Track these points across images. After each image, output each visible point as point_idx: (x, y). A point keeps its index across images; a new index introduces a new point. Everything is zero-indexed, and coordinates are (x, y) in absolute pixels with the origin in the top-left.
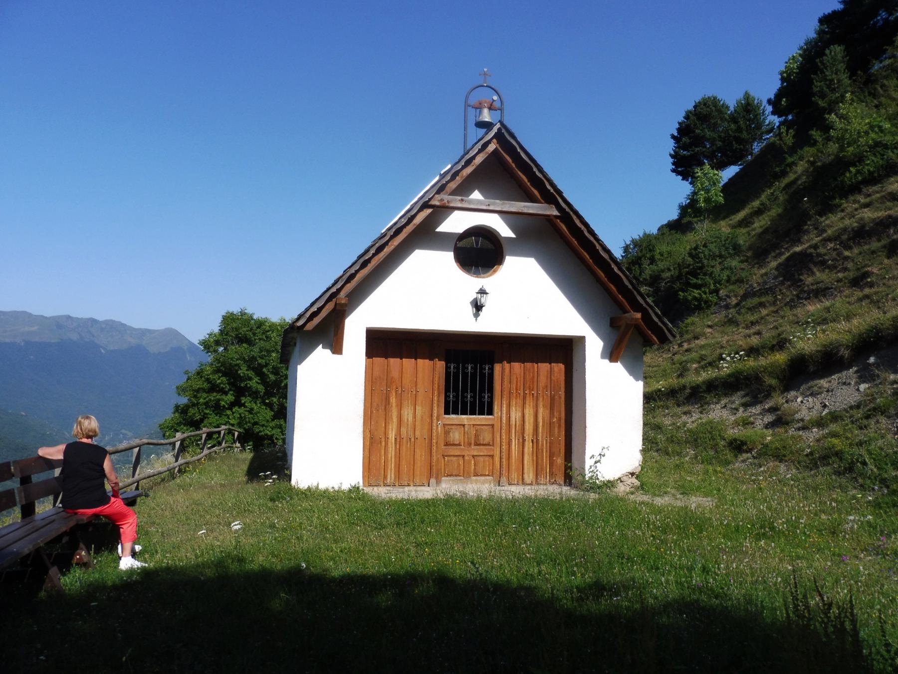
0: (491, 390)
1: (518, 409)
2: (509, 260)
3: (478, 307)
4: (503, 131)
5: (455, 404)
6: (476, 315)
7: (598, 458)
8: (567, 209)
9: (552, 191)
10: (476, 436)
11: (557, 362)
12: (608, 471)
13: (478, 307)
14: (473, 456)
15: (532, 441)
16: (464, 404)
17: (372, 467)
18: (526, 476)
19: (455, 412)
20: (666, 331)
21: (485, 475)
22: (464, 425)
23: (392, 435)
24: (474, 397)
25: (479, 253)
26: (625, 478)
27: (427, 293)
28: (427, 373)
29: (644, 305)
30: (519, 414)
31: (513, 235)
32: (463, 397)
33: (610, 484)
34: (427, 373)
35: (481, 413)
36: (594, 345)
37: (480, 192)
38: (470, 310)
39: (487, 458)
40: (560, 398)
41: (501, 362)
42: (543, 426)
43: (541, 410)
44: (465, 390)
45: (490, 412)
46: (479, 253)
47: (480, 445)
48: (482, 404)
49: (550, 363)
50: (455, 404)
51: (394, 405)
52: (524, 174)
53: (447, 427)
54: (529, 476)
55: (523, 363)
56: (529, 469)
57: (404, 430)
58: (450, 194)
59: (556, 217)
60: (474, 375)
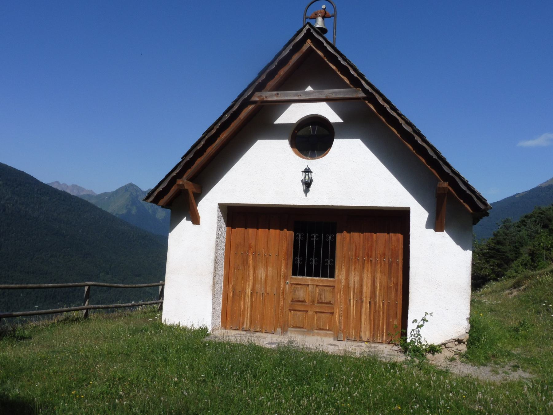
0: (333, 257)
1: (354, 275)
2: (337, 143)
3: (307, 185)
4: (312, 30)
5: (302, 266)
6: (306, 191)
7: (421, 323)
8: (370, 90)
9: (356, 75)
10: (320, 295)
11: (395, 232)
12: (430, 336)
13: (307, 185)
14: (316, 312)
15: (370, 303)
16: (309, 267)
17: (229, 315)
18: (363, 334)
19: (302, 274)
20: (475, 199)
21: (326, 330)
22: (308, 285)
23: (249, 290)
24: (318, 262)
25: (312, 139)
26: (450, 345)
27: (266, 173)
28: (280, 240)
29: (451, 174)
30: (357, 279)
31: (340, 121)
32: (309, 261)
33: (433, 349)
34: (280, 240)
35: (324, 275)
36: (419, 216)
37: (311, 86)
38: (301, 187)
39: (328, 315)
40: (397, 264)
41: (341, 232)
42: (380, 290)
43: (378, 276)
44: (310, 255)
45: (332, 275)
46: (312, 139)
47: (322, 303)
48: (325, 268)
49: (388, 233)
50: (302, 266)
51: (251, 265)
52: (334, 65)
53: (294, 286)
54: (366, 334)
55: (362, 233)
56: (365, 328)
57: (257, 286)
58: (270, 91)
59: (364, 98)
60: (318, 243)
